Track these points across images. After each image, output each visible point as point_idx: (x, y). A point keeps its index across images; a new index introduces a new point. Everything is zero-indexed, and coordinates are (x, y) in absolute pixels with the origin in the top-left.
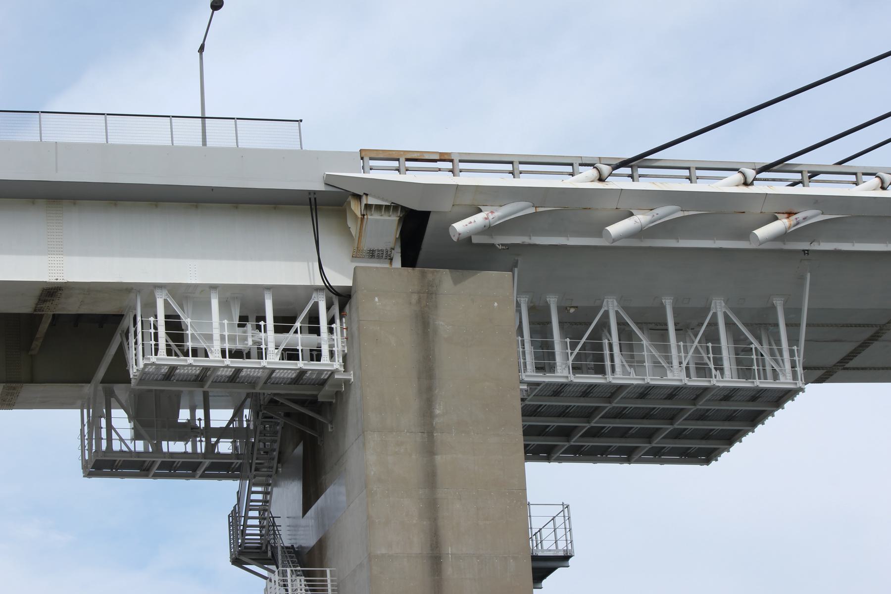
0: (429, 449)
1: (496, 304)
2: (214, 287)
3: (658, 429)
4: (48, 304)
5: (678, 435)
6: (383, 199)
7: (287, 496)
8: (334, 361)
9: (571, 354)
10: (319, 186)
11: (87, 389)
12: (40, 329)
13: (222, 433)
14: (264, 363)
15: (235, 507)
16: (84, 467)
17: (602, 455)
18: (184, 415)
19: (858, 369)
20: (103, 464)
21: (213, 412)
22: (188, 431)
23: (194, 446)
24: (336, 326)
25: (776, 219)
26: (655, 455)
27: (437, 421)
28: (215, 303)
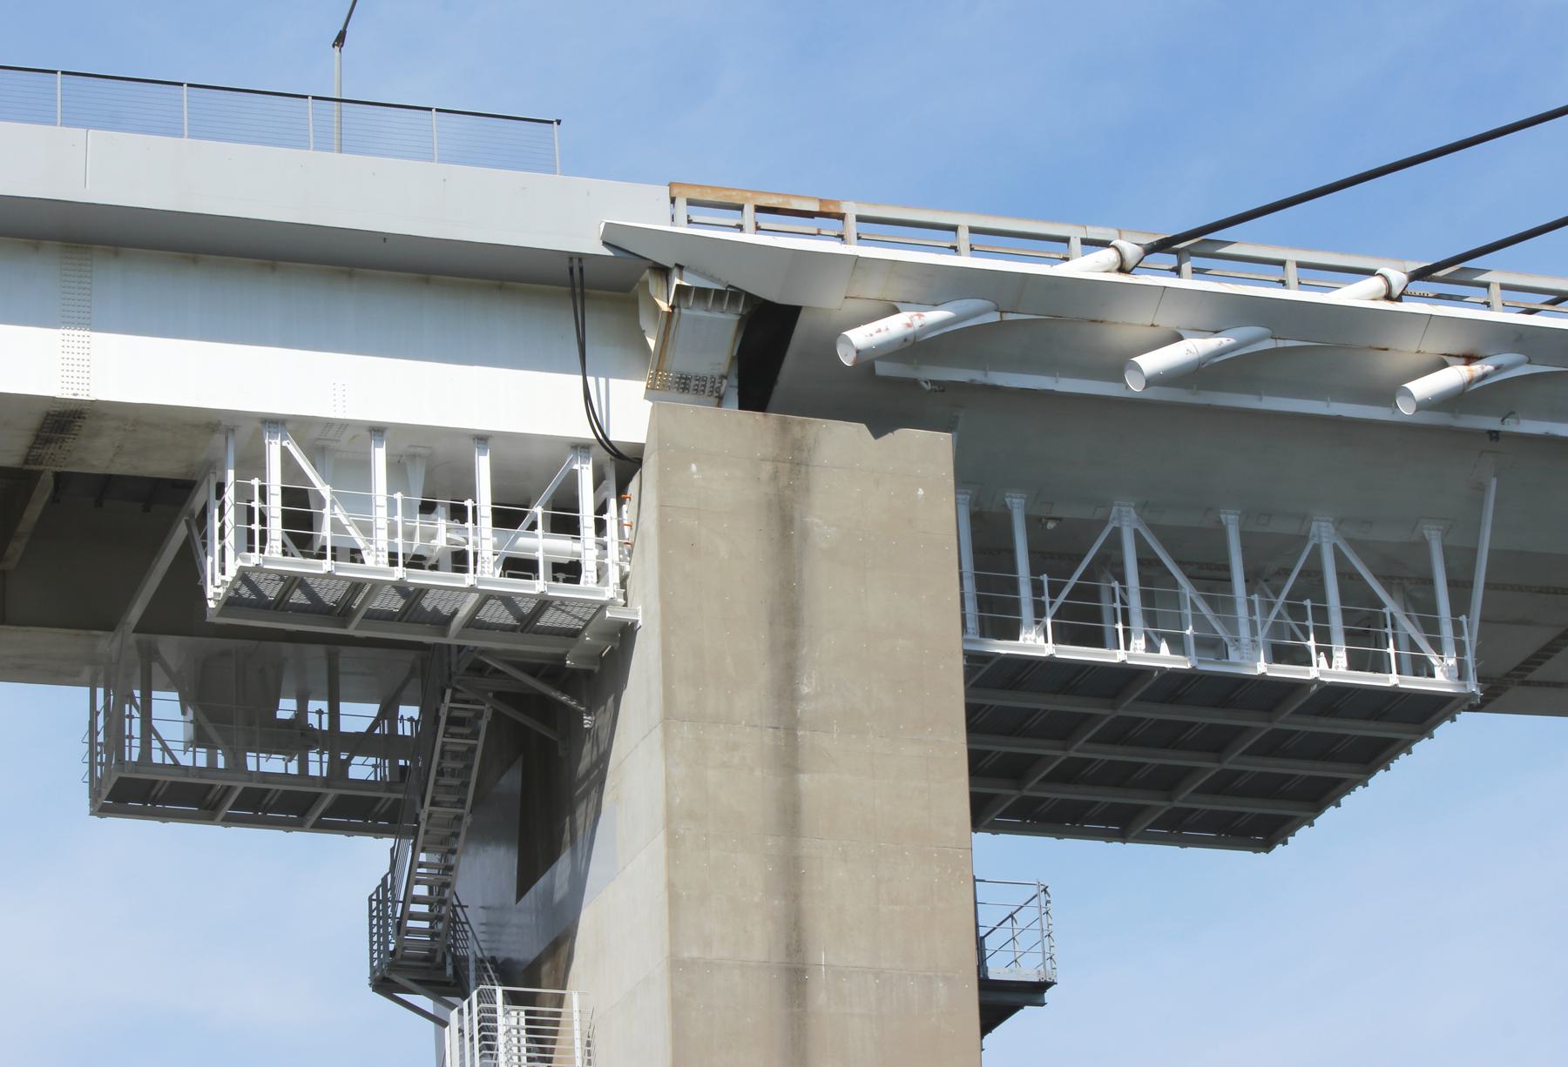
0: (788, 759)
1: (921, 492)
2: (377, 431)
3: (1192, 770)
4: (52, 448)
5: (1223, 785)
6: (712, 278)
7: (484, 874)
8: (606, 584)
9: (1051, 604)
10: (591, 244)
11: (106, 644)
12: (26, 515)
13: (360, 744)
14: (468, 579)
15: (384, 880)
16: (94, 794)
17: (1073, 823)
18: (287, 708)
19: (1547, 684)
20: (129, 791)
21: (344, 707)
22: (296, 738)
23: (304, 765)
24: (610, 517)
25: (1445, 365)
26: (1171, 828)
27: (804, 708)
28: (379, 456)
